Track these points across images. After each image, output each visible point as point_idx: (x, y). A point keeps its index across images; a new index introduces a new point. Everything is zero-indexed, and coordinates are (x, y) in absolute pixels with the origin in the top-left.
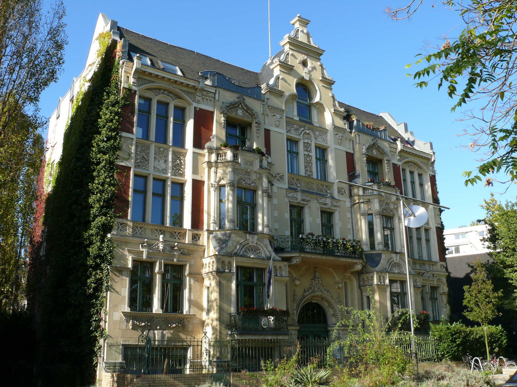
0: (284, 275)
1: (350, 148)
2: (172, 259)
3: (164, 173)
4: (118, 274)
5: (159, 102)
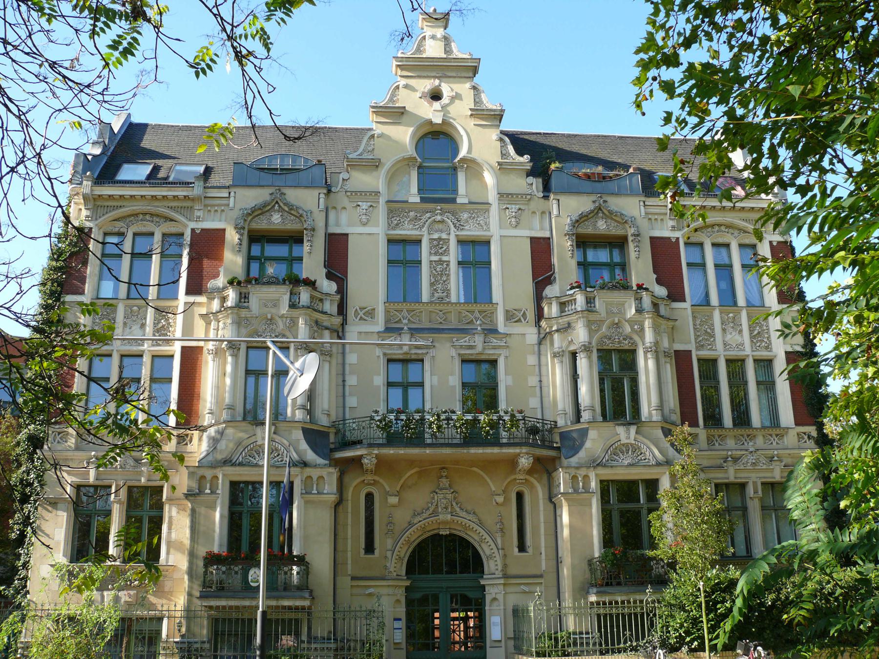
0: (325, 492)
1: (542, 229)
2: (138, 478)
3: (741, 350)
4: (50, 508)
5: (741, 246)
